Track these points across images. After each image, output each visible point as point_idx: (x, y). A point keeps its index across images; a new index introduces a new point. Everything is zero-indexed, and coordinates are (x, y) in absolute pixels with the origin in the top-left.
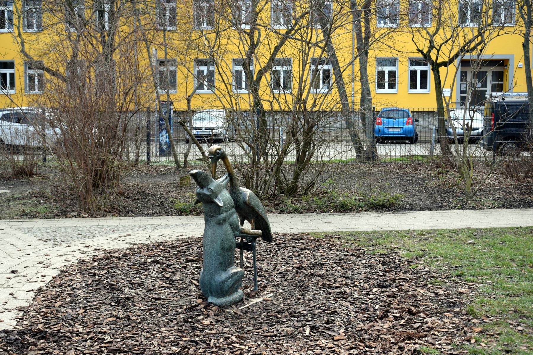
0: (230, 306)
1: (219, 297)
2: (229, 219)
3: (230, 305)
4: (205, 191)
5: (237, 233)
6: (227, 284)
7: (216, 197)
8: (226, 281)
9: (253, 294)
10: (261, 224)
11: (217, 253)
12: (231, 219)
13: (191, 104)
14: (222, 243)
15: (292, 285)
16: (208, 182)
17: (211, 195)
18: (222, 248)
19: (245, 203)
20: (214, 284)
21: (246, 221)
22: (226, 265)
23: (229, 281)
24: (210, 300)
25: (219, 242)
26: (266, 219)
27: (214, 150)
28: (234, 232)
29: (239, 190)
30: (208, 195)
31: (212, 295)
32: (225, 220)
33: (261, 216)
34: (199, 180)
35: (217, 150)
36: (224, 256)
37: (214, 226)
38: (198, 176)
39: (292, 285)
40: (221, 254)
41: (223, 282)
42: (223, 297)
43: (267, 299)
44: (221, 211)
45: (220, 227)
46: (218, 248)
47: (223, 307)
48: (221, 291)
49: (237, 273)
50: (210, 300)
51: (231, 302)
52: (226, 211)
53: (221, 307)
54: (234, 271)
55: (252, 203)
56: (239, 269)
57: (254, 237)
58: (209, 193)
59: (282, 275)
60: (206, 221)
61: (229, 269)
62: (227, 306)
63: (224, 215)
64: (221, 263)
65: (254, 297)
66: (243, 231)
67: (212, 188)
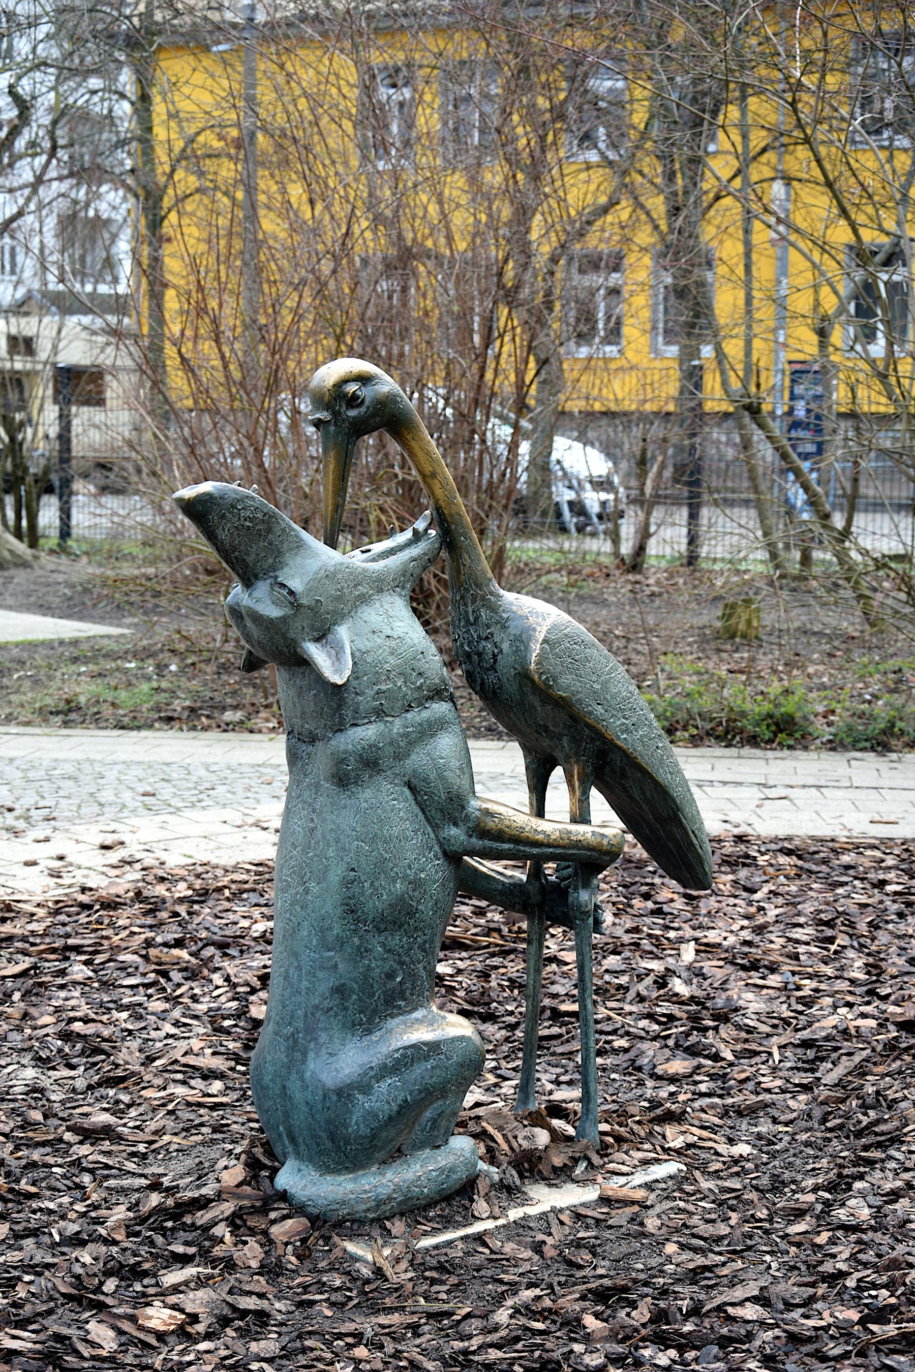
0: (379, 1221)
1: (327, 1169)
2: (400, 756)
3: (369, 1222)
4: (263, 602)
5: (455, 833)
6: (365, 1103)
7: (322, 636)
8: (363, 1085)
9: (558, 1161)
10: (636, 795)
11: (323, 932)
12: (418, 759)
13: (811, 300)
14: (348, 883)
15: (824, 1120)
16: (279, 553)
17: (284, 619)
18: (352, 910)
19: (524, 675)
20: (298, 1096)
21: (558, 773)
22: (374, 1001)
23: (383, 1086)
24: (286, 1179)
25: (336, 874)
26: (663, 777)
27: (330, 381)
28: (436, 827)
29: (494, 609)
30: (271, 621)
31: (298, 1155)
32: (370, 763)
33: (624, 753)
34: (223, 535)
35: (346, 381)
36: (362, 952)
37: (317, 786)
38: (214, 517)
39: (824, 1120)
40: (341, 943)
41: (344, 1094)
42: (348, 1170)
43: (625, 1192)
44: (348, 713)
45: (343, 799)
46: (328, 907)
47: (339, 1224)
48: (332, 1138)
49: (434, 1047)
50: (286, 1179)
51: (379, 1203)
52: (380, 713)
53: (325, 1224)
54: (422, 1035)
55: (566, 680)
56: (458, 1027)
57: (589, 861)
58: (273, 612)
59: (811, 1054)
60: (293, 757)
61: (392, 1023)
62: (361, 1222)
63: (367, 733)
64: (340, 991)
65: (561, 1175)
66: (491, 824)
67: (296, 584)
